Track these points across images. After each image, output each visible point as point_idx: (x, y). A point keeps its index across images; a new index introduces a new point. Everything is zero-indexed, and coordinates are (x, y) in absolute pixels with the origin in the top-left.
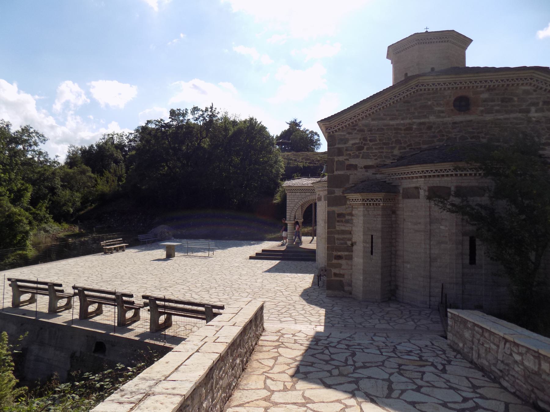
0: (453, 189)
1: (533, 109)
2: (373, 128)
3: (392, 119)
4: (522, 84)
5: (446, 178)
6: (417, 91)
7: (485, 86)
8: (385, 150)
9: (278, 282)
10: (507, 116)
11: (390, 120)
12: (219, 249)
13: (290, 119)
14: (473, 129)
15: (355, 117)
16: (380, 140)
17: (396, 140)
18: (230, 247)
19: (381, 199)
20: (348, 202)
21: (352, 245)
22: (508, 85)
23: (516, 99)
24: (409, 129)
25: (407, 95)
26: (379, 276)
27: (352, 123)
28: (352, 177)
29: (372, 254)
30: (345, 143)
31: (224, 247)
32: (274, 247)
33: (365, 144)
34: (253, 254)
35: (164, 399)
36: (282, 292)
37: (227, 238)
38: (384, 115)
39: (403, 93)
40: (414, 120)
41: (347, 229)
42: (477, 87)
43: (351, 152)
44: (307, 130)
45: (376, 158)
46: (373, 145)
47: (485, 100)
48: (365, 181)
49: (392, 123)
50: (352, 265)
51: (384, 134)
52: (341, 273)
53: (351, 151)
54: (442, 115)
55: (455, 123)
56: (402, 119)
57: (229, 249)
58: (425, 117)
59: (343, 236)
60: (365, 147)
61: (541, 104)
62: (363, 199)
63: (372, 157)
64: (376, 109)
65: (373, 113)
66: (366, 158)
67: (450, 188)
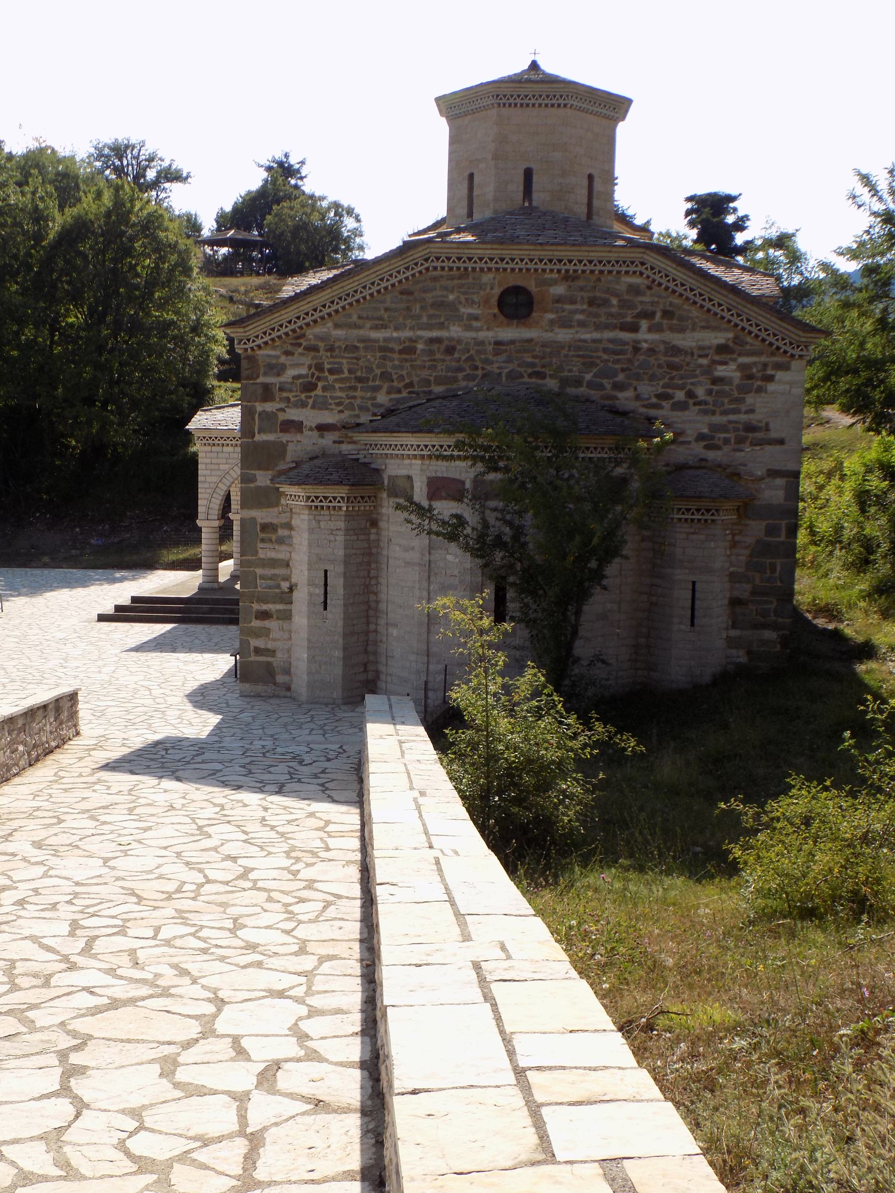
0: (468, 485)
1: (644, 324)
2: (337, 345)
3: (376, 328)
4: (627, 272)
5: (458, 463)
6: (427, 269)
7: (559, 271)
8: (358, 393)
9: (151, 671)
10: (596, 335)
11: (371, 328)
12: (19, 595)
14: (533, 357)
15: (298, 318)
16: (350, 371)
17: (382, 373)
18: (52, 588)
19: (342, 498)
20: (283, 501)
21: (291, 589)
22: (601, 272)
23: (615, 301)
24: (408, 350)
25: (407, 279)
26: (338, 654)
27: (294, 331)
28: (290, 448)
29: (325, 609)
30: (278, 375)
31: (35, 589)
32: (164, 591)
33: (319, 379)
34: (109, 609)
36: (150, 690)
37: (46, 559)
38: (360, 317)
39: (399, 272)
40: (419, 333)
41: (280, 556)
42: (544, 270)
43: (290, 395)
44: (322, 198)
45: (341, 408)
46: (335, 380)
47: (559, 300)
48: (317, 457)
49: (374, 335)
50: (290, 632)
51: (358, 359)
52: (269, 647)
53: (291, 391)
54: (476, 324)
55: (498, 343)
56: (396, 329)
57: (48, 595)
58: (442, 326)
59: (273, 571)
60: (320, 384)
61: (658, 315)
62: (309, 497)
63: (333, 406)
64: (342, 304)
65: (337, 311)
66: (320, 409)
67: (463, 483)
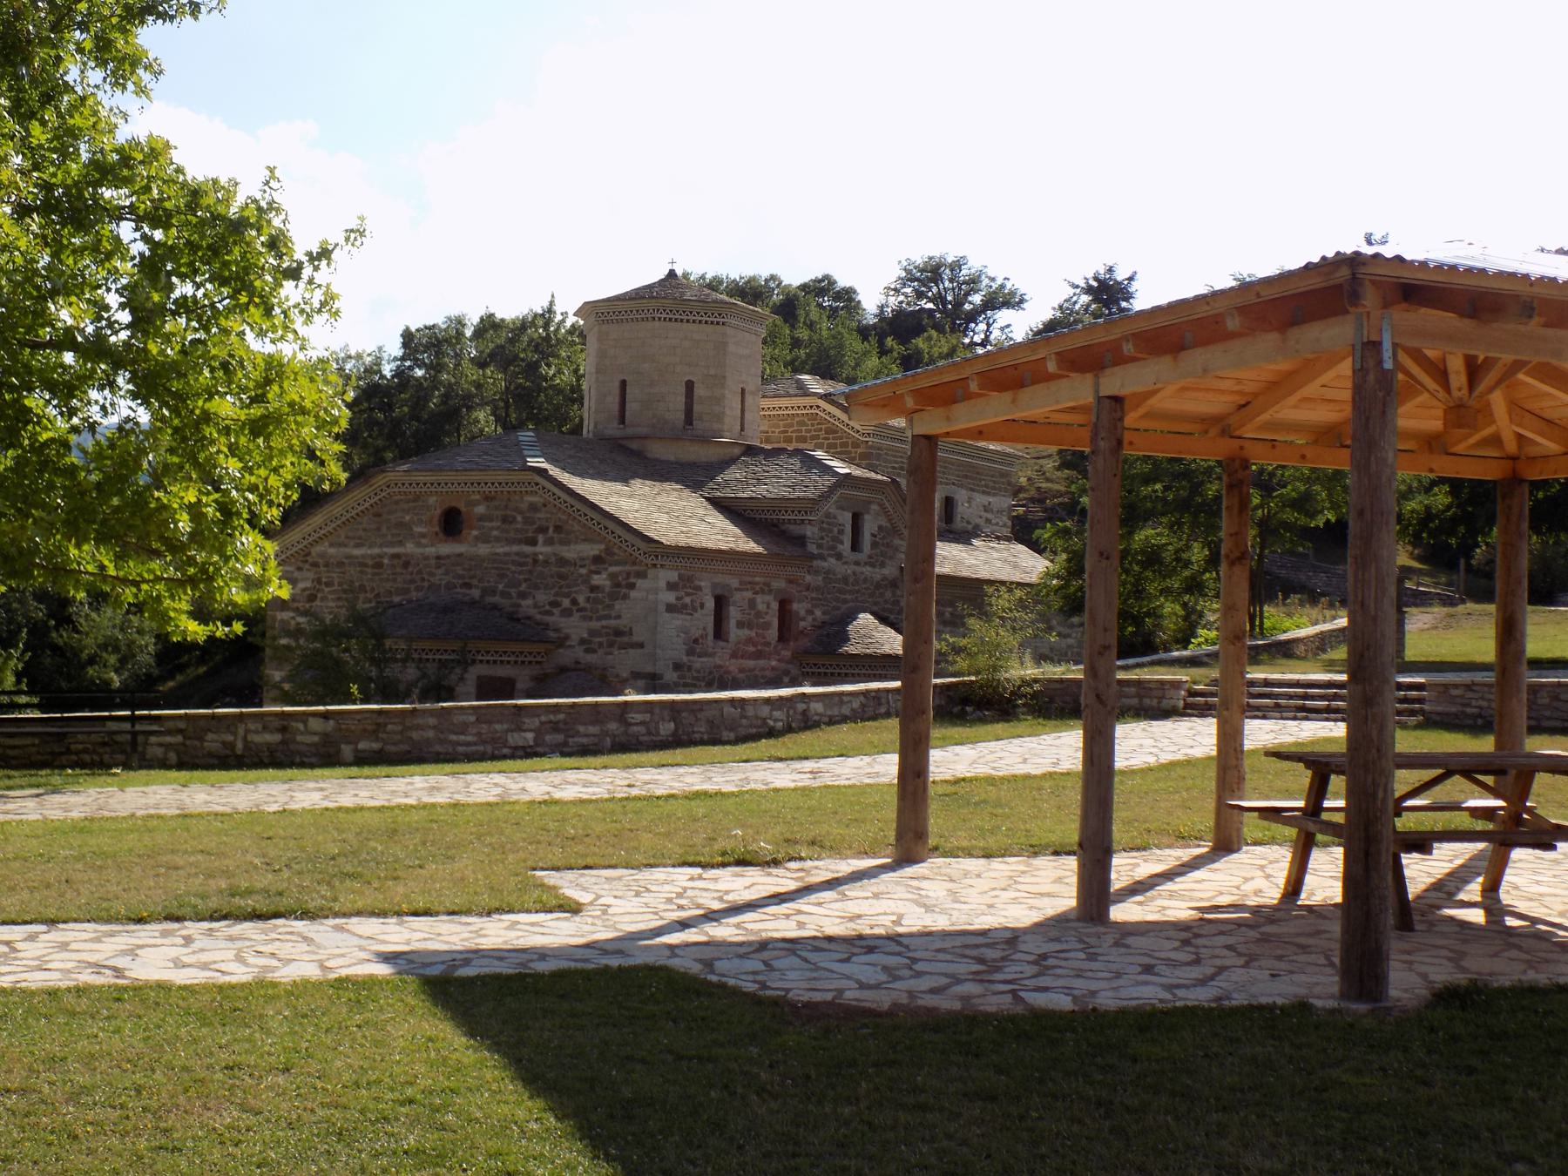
3: (357, 546)
10: (507, 549)
13: (1086, 269)
23: (519, 518)
35: (132, 952)
47: (481, 518)
49: (357, 552)
55: (438, 558)
58: (401, 543)
